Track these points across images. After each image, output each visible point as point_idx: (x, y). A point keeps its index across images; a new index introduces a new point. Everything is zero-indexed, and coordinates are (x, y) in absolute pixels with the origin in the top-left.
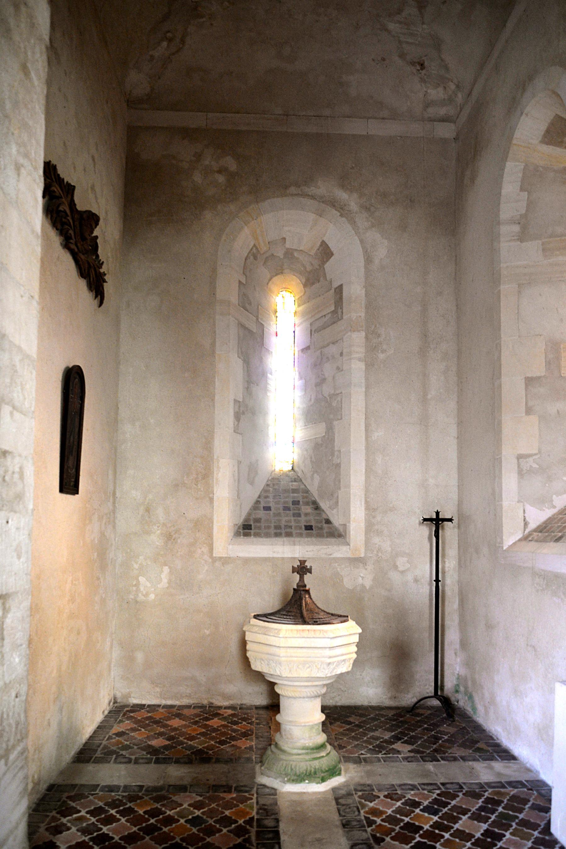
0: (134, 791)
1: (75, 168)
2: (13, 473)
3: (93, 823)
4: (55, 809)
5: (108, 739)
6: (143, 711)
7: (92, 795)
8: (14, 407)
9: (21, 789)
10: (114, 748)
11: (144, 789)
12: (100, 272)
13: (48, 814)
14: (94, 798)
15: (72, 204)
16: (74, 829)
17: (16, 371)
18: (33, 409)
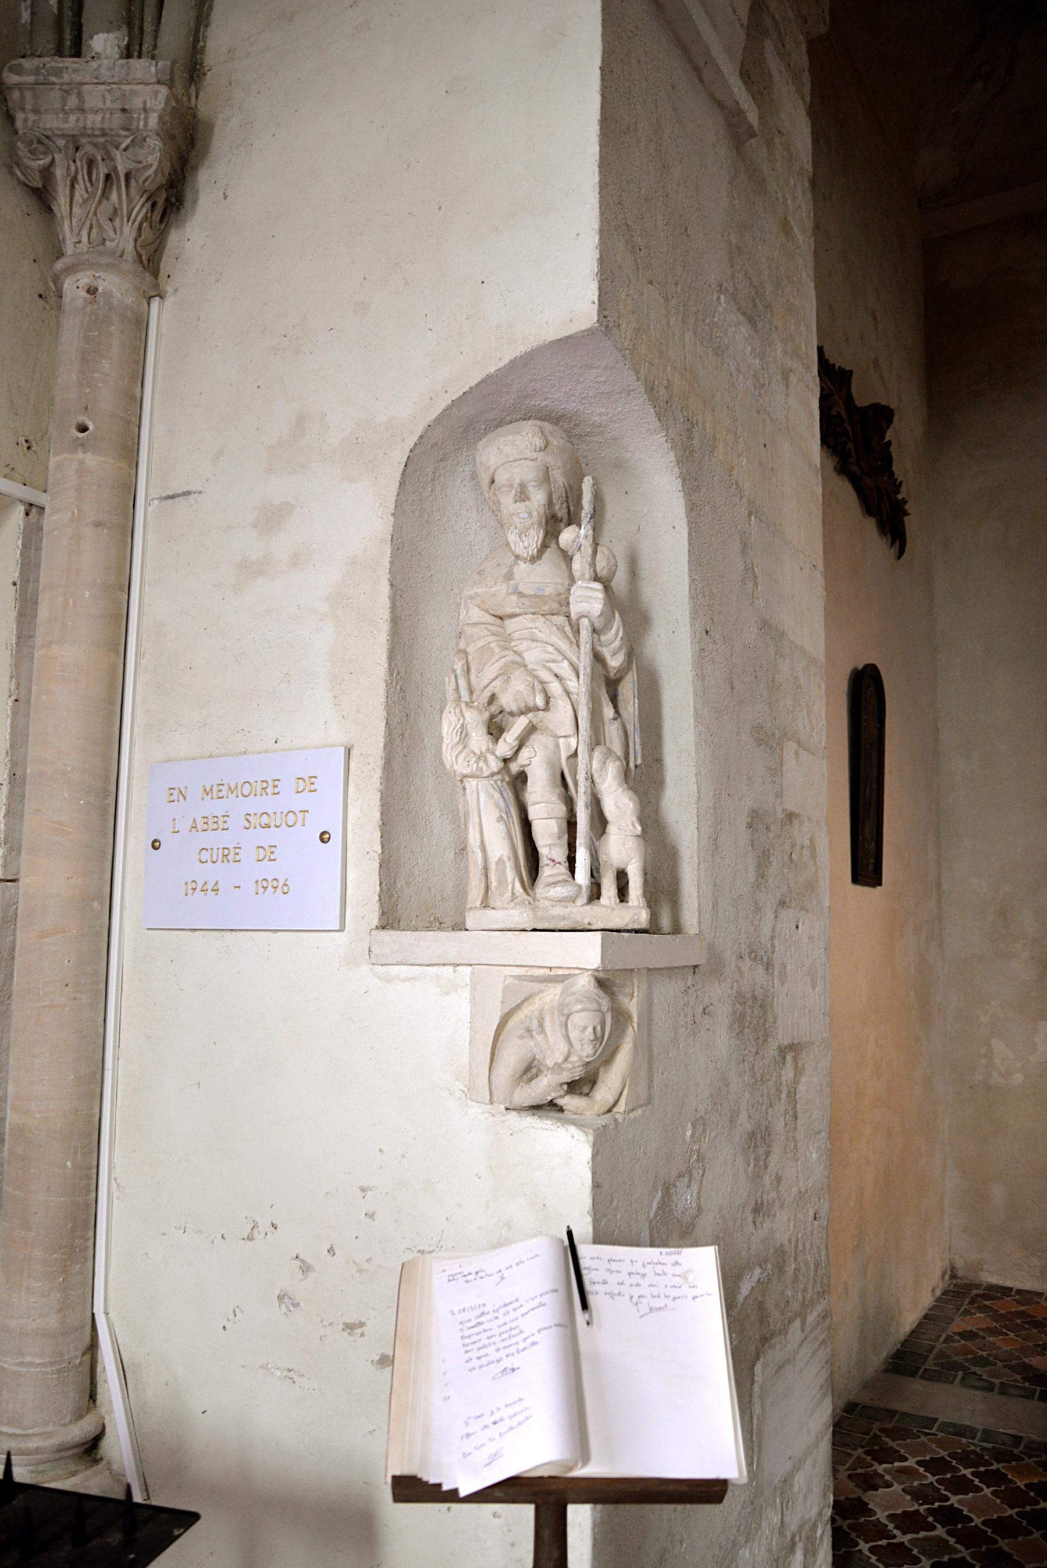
0: (1004, 1444)
1: (847, 340)
2: (803, 847)
3: (932, 1483)
4: (862, 1447)
5: (945, 1341)
6: (1008, 1299)
7: (927, 1434)
8: (799, 743)
9: (821, 1380)
10: (959, 1359)
11: (1023, 1443)
12: (897, 499)
13: (850, 1451)
14: (929, 1440)
15: (849, 399)
16: (897, 1487)
17: (800, 687)
18: (823, 744)
